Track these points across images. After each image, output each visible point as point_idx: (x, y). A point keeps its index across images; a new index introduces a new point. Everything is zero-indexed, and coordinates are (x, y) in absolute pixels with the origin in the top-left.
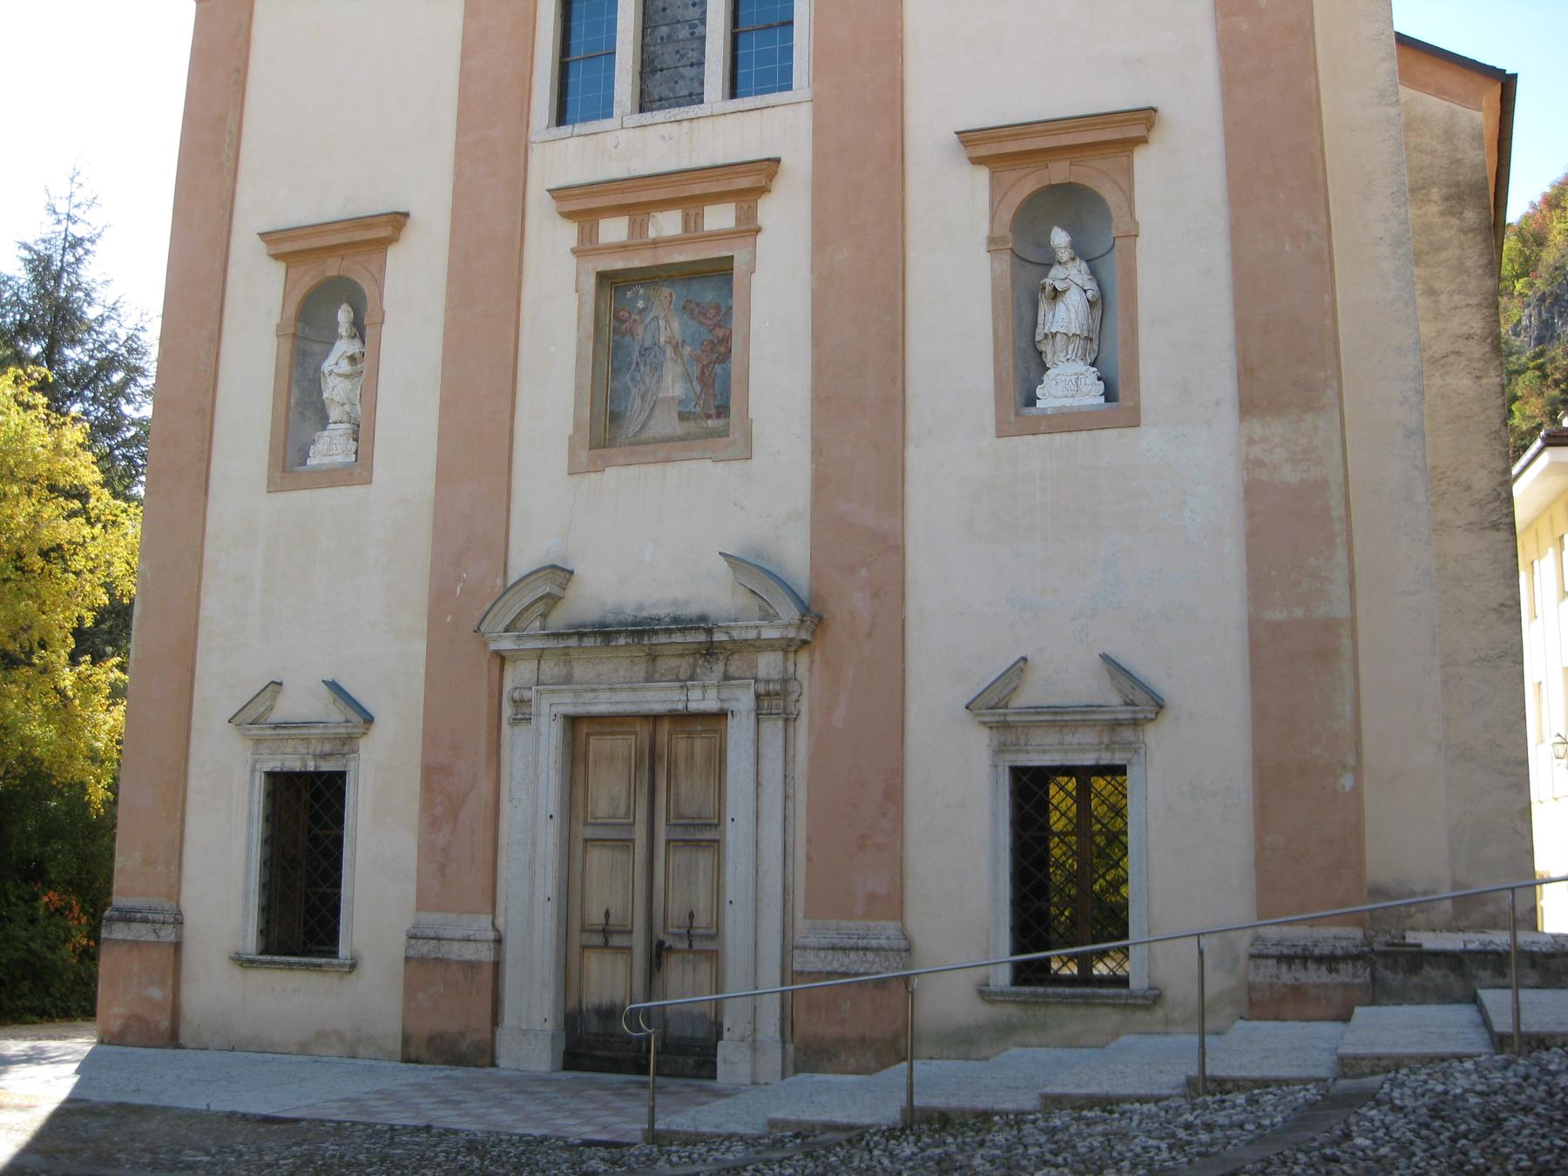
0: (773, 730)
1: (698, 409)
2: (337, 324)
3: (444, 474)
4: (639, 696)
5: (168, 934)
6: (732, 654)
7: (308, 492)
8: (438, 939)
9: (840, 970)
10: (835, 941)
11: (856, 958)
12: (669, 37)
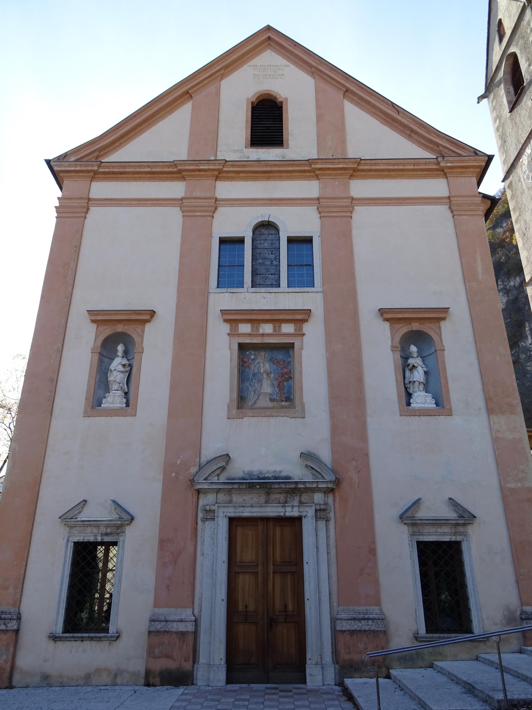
0: (322, 524)
1: (278, 398)
2: (117, 351)
3: (172, 413)
4: (263, 509)
5: (13, 625)
6: (303, 493)
7: (104, 418)
8: (166, 621)
9: (357, 629)
10: (354, 616)
11: (364, 623)
12: (263, 263)
